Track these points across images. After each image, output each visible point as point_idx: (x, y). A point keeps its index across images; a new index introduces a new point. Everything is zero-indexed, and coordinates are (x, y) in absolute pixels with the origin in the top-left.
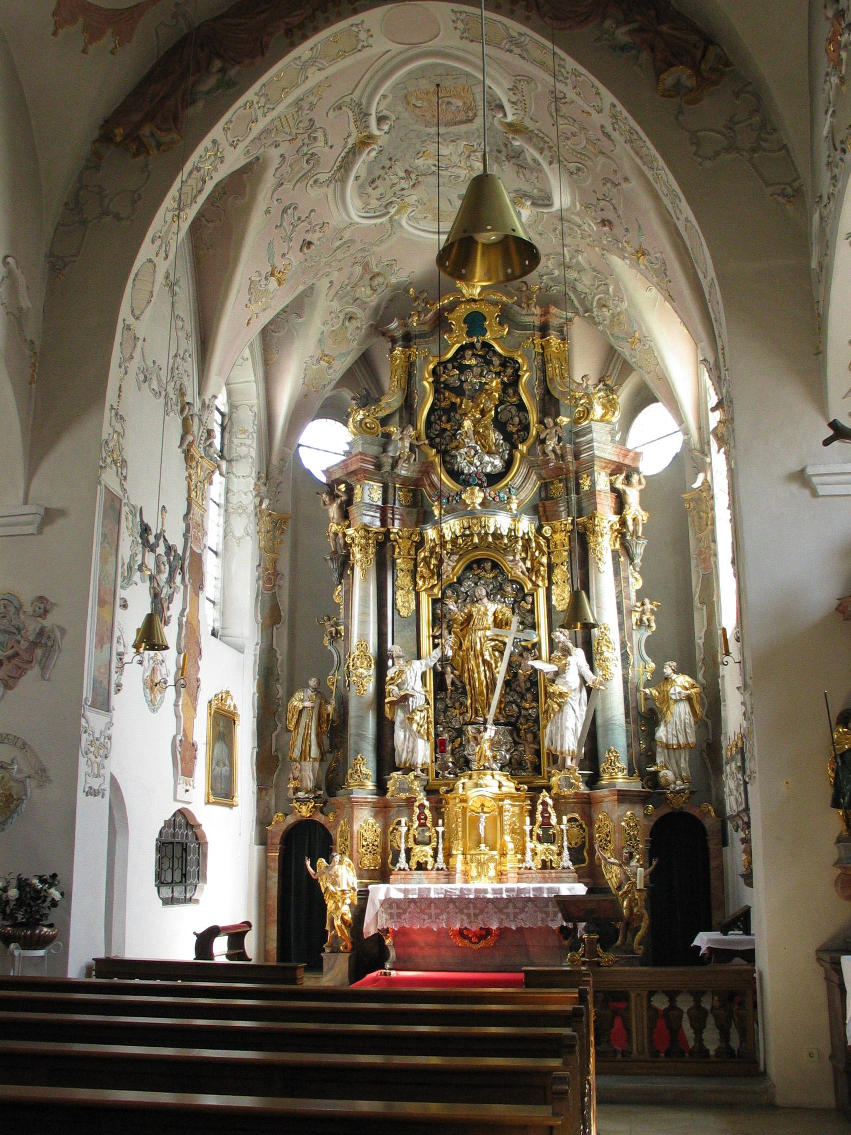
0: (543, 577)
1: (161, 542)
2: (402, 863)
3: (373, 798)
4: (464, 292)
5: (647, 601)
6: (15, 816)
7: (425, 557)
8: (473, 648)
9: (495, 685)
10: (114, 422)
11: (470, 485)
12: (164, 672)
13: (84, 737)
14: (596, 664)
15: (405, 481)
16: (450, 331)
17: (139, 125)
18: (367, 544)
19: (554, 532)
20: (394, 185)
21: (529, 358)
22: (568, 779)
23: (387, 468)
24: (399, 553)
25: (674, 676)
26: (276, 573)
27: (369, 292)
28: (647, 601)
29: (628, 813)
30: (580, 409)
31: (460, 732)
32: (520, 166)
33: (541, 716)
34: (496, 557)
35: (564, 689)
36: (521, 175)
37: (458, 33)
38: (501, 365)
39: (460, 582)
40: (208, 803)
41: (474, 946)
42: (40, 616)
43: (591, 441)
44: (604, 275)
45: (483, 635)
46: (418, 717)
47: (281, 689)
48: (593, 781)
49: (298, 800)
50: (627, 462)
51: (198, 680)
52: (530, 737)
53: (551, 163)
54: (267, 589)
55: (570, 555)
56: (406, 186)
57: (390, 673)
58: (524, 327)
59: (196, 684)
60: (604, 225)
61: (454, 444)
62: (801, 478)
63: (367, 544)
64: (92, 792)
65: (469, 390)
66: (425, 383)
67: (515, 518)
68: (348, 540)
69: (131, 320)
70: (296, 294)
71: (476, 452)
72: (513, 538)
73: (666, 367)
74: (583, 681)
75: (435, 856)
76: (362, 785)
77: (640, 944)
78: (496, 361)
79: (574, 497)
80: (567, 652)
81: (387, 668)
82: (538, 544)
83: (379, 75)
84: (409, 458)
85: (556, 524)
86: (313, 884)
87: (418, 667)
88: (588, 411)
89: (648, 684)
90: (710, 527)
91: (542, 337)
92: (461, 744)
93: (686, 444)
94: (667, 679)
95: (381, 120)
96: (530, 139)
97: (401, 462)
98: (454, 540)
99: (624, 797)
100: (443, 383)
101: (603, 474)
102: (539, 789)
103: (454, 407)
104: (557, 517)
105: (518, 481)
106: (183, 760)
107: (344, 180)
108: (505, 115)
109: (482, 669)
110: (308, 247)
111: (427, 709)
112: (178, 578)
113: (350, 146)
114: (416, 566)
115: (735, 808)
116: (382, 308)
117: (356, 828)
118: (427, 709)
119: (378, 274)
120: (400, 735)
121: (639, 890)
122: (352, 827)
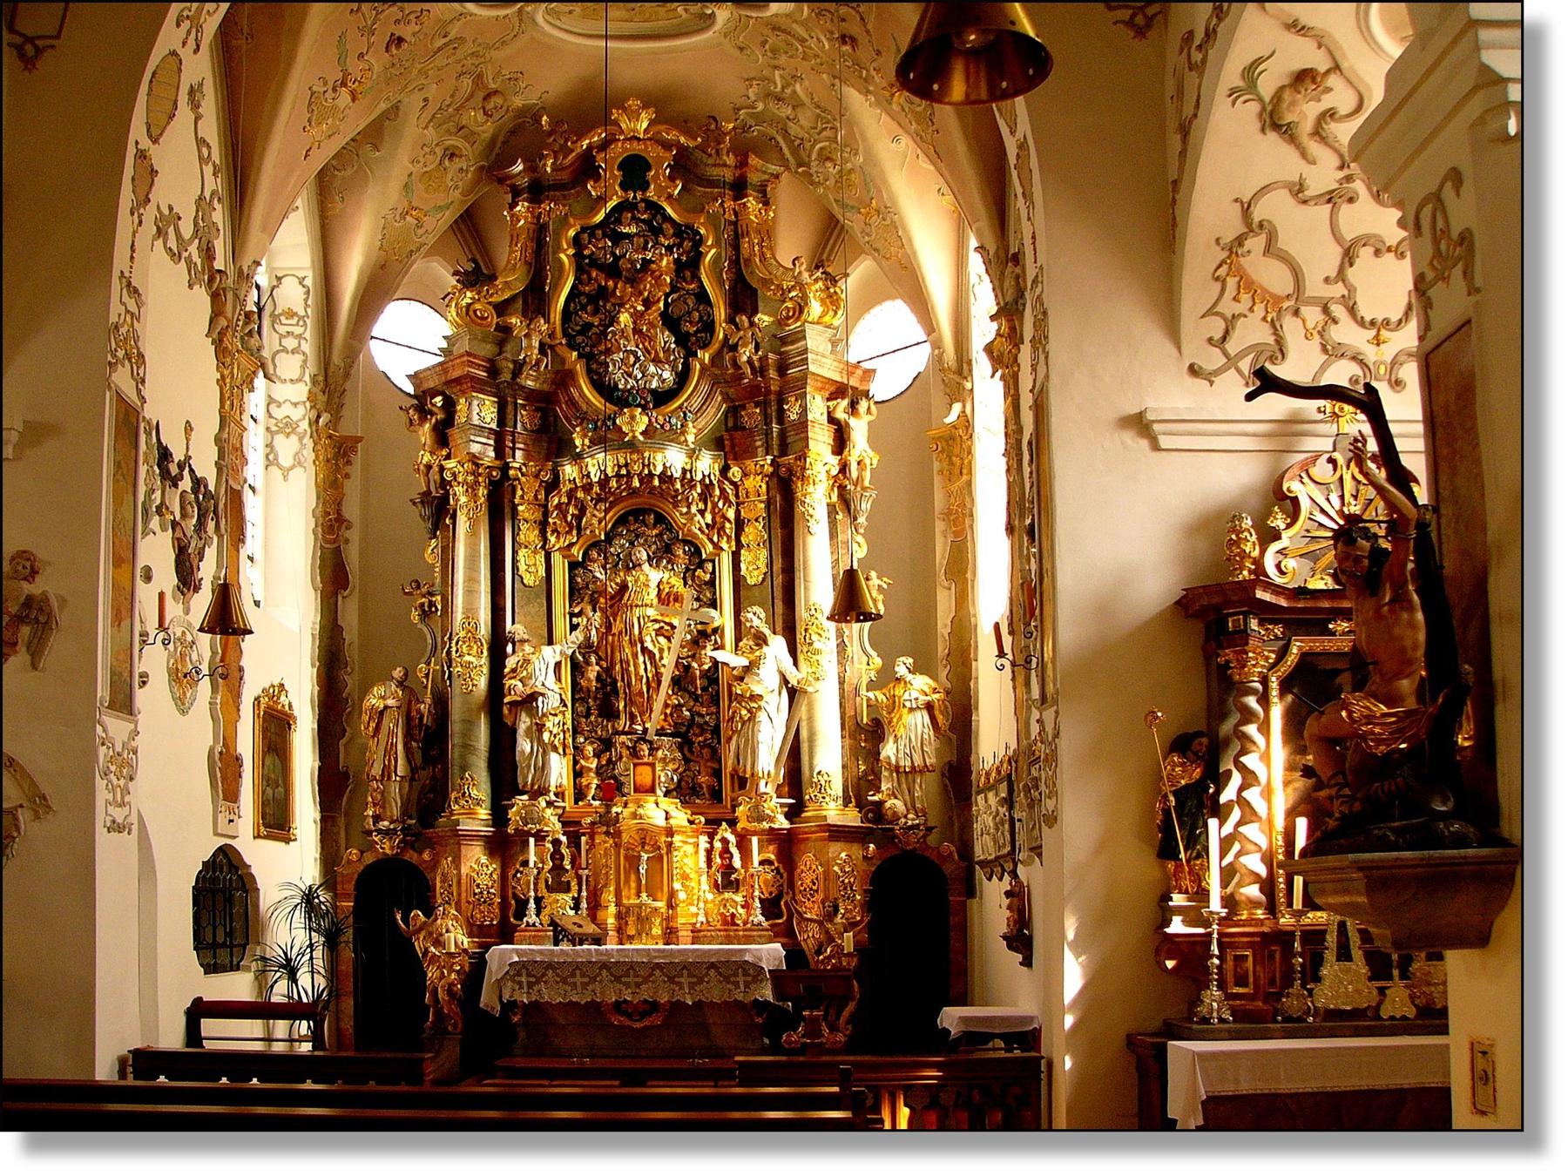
0: (729, 537)
1: (186, 472)
2: (531, 917)
4: (623, 126)
5: (873, 574)
7: (560, 504)
8: (628, 629)
9: (659, 683)
10: (126, 298)
11: (628, 405)
12: (195, 657)
13: (102, 750)
14: (801, 657)
15: (531, 395)
16: (597, 178)
18: (477, 483)
19: (745, 475)
21: (716, 228)
23: (506, 376)
24: (522, 497)
25: (909, 677)
26: (340, 519)
27: (481, 117)
28: (873, 574)
29: (843, 855)
30: (789, 304)
33: (723, 726)
35: (757, 690)
38: (674, 235)
39: (609, 539)
40: (258, 836)
42: (25, 579)
44: (833, 117)
45: (646, 610)
47: (351, 682)
49: (379, 831)
51: (241, 669)
54: (327, 541)
55: (768, 507)
57: (511, 663)
58: (712, 183)
59: (237, 675)
60: (845, 43)
62: (1140, 424)
63: (477, 483)
64: (116, 827)
65: (628, 270)
66: (562, 256)
68: (448, 476)
69: (145, 143)
70: (372, 117)
71: (637, 359)
72: (689, 483)
73: (915, 253)
74: (785, 681)
75: (576, 907)
76: (471, 814)
77: (848, 1023)
79: (775, 427)
80: (761, 640)
81: (505, 656)
82: (723, 491)
84: (538, 362)
85: (750, 465)
86: (404, 944)
87: (550, 654)
88: (800, 309)
89: (871, 686)
90: (965, 478)
91: (736, 199)
92: (609, 761)
93: (937, 359)
97: (526, 369)
99: (838, 833)
100: (589, 257)
101: (818, 398)
102: (718, 822)
103: (603, 293)
104: (751, 453)
105: (696, 403)
106: (224, 779)
109: (641, 659)
110: (398, 45)
111: (563, 713)
112: (211, 525)
114: (546, 514)
115: (992, 850)
116: (499, 144)
117: (464, 870)
118: (563, 713)
119: (496, 92)
120: (524, 745)
121: (849, 954)
122: (458, 868)
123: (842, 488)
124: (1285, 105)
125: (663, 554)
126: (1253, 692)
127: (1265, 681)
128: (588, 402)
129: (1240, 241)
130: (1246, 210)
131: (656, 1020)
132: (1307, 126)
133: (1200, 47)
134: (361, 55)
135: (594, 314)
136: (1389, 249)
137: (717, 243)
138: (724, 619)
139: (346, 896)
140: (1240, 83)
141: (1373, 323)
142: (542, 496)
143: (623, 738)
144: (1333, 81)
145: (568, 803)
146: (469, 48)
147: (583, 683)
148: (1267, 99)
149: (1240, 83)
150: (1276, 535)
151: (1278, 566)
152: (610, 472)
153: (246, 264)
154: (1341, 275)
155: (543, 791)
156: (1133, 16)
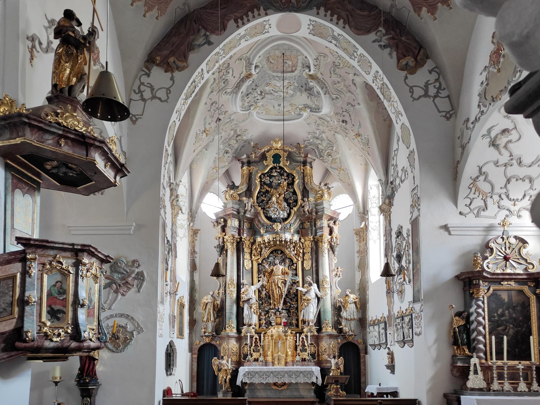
3: (236, 335)
6: (129, 346)
8: (274, 282)
14: (321, 290)
15: (248, 219)
16: (266, 160)
17: (167, 57)
18: (233, 242)
20: (255, 97)
22: (309, 330)
27: (235, 142)
31: (268, 312)
32: (310, 94)
34: (283, 249)
35: (310, 298)
36: (310, 98)
37: (309, 31)
41: (279, 389)
43: (324, 208)
44: (331, 144)
45: (278, 278)
46: (254, 306)
47: (197, 295)
48: (319, 330)
49: (205, 336)
50: (335, 216)
52: (295, 314)
53: (325, 94)
55: (312, 249)
56: (259, 98)
57: (242, 290)
61: (267, 206)
62: (446, 228)
67: (293, 235)
71: (277, 210)
74: (317, 296)
78: (285, 174)
79: (314, 228)
80: (310, 285)
81: (241, 289)
83: (261, 45)
84: (251, 210)
85: (307, 238)
87: (254, 288)
88: (322, 196)
94: (347, 295)
95: (256, 67)
96: (318, 82)
97: (248, 212)
98: (269, 242)
99: (331, 336)
103: (267, 192)
104: (307, 235)
107: (237, 93)
108: (310, 71)
113: (241, 77)
114: (251, 251)
117: (230, 346)
119: (239, 135)
120: (246, 312)
123: (331, 244)
124: (497, 139)
125: (283, 261)
126: (481, 300)
127: (483, 298)
128: (264, 221)
129: (477, 177)
130: (480, 169)
131: (285, 387)
132: (503, 145)
133: (472, 123)
134: (210, 124)
135: (265, 197)
136: (521, 179)
137: (299, 178)
138: (300, 279)
139: (195, 354)
140: (486, 133)
141: (513, 200)
142: (250, 246)
143: (272, 310)
144: (514, 132)
145: (257, 328)
146: (235, 122)
147: (261, 296)
148: (493, 137)
149: (486, 133)
150: (486, 258)
151: (487, 266)
152: (271, 240)
153: (178, 181)
154: (505, 186)
155: (250, 325)
156: (446, 114)
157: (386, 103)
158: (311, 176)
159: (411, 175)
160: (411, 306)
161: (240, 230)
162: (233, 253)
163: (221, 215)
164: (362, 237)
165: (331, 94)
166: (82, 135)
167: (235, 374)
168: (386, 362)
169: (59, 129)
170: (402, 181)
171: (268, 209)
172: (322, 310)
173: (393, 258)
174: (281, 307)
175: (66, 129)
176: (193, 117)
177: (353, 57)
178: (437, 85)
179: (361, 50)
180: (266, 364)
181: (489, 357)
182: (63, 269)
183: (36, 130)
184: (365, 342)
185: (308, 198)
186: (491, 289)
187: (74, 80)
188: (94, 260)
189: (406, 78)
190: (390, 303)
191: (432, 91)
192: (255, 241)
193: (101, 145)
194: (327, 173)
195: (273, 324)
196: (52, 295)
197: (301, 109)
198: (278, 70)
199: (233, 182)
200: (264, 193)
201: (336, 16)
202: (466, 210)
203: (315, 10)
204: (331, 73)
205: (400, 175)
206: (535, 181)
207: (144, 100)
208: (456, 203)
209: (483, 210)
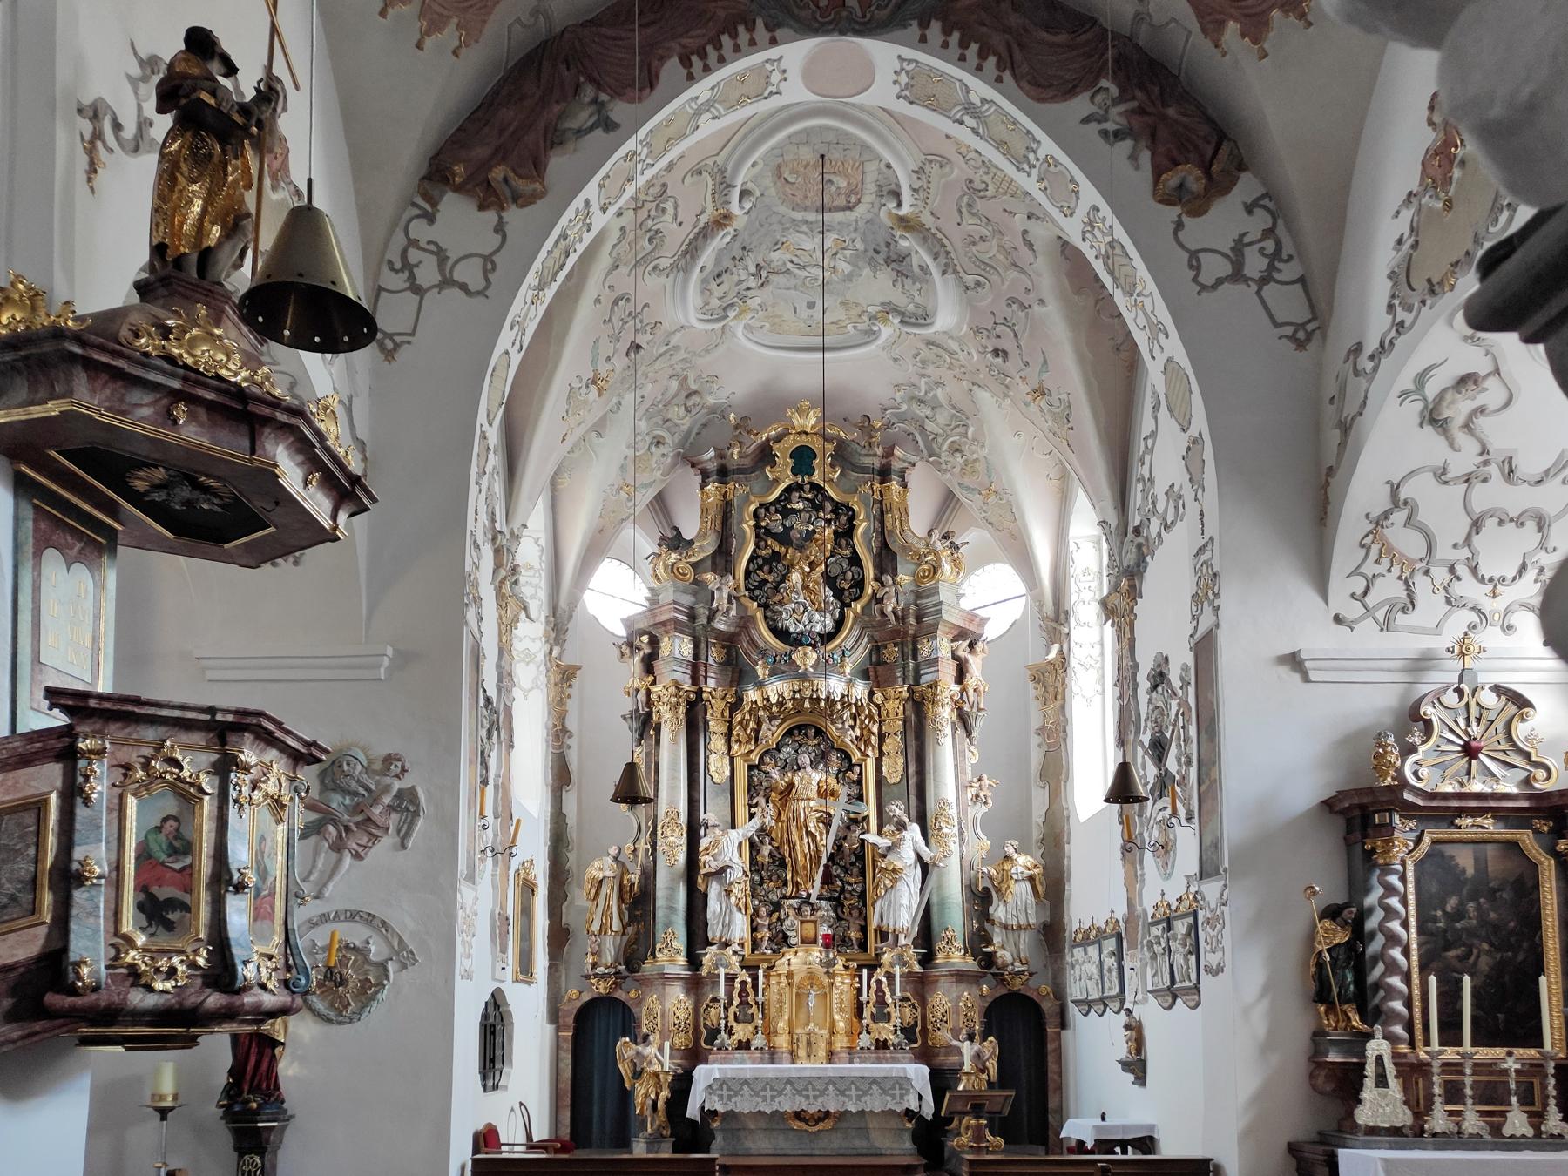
3: (686, 974)
6: (375, 1004)
8: (796, 818)
14: (932, 841)
15: (720, 635)
16: (774, 464)
17: (486, 165)
18: (678, 703)
20: (740, 282)
22: (898, 959)
27: (682, 411)
31: (777, 906)
32: (901, 273)
34: (821, 723)
35: (899, 865)
36: (899, 285)
37: (897, 89)
43: (940, 603)
44: (961, 418)
45: (808, 806)
46: (736, 889)
47: (572, 858)
48: (927, 960)
49: (596, 975)
50: (972, 628)
52: (856, 913)
53: (944, 273)
55: (905, 722)
56: (752, 285)
57: (704, 843)
61: (776, 599)
62: (1294, 661)
67: (850, 683)
71: (806, 609)
74: (919, 858)
78: (828, 506)
79: (912, 663)
80: (901, 826)
81: (699, 838)
83: (758, 132)
84: (728, 610)
85: (890, 691)
87: (736, 836)
88: (935, 570)
94: (1007, 858)
95: (744, 194)
96: (925, 239)
97: (719, 616)
98: (780, 704)
99: (961, 976)
103: (776, 556)
104: (893, 683)
107: (687, 270)
108: (900, 205)
113: (701, 225)
114: (730, 729)
117: (668, 1005)
119: (695, 392)
120: (714, 906)
123: (960, 709)
124: (1445, 404)
125: (822, 758)
126: (1396, 872)
127: (1404, 864)
128: (766, 642)
129: (1386, 515)
130: (1395, 490)
131: (828, 1124)
132: (1460, 420)
133: (1372, 357)
134: (608, 359)
135: (770, 572)
136: (1511, 520)
137: (867, 518)
138: (871, 810)
139: (566, 1028)
140: (1411, 386)
141: (1491, 580)
142: (727, 714)
143: (791, 902)
144: (1492, 383)
145: (747, 951)
146: (682, 355)
147: (759, 859)
148: (1430, 399)
149: (1411, 386)
150: (1413, 749)
151: (1415, 773)
152: (786, 695)
153: (516, 526)
154: (1468, 541)
155: (727, 944)
156: (1295, 332)
157: (1120, 300)
158: (904, 512)
159: (1192, 509)
160: (1193, 889)
161: (696, 669)
162: (675, 734)
163: (642, 625)
164: (1051, 689)
165: (962, 274)
166: (239, 393)
167: (682, 1085)
168: (1122, 1050)
169: (173, 375)
170: (1167, 527)
171: (778, 608)
172: (934, 900)
173: (1140, 751)
174: (815, 892)
175: (192, 374)
176: (562, 340)
177: (1026, 167)
178: (1270, 245)
179: (1048, 147)
180: (772, 1056)
181: (1419, 1036)
182: (184, 781)
183: (104, 377)
184: (1059, 994)
185: (894, 574)
186: (1427, 840)
187: (216, 231)
188: (272, 754)
189: (1179, 225)
190: (1133, 880)
191: (1255, 264)
192: (740, 700)
193: (293, 421)
194: (948, 502)
195: (793, 941)
196: (150, 857)
197: (873, 318)
198: (808, 203)
199: (676, 529)
200: (767, 561)
201: (974, 47)
202: (1353, 610)
203: (914, 29)
204: (960, 212)
205: (1160, 507)
206: (1554, 526)
207: (417, 290)
208: (1323, 589)
209: (1404, 610)
